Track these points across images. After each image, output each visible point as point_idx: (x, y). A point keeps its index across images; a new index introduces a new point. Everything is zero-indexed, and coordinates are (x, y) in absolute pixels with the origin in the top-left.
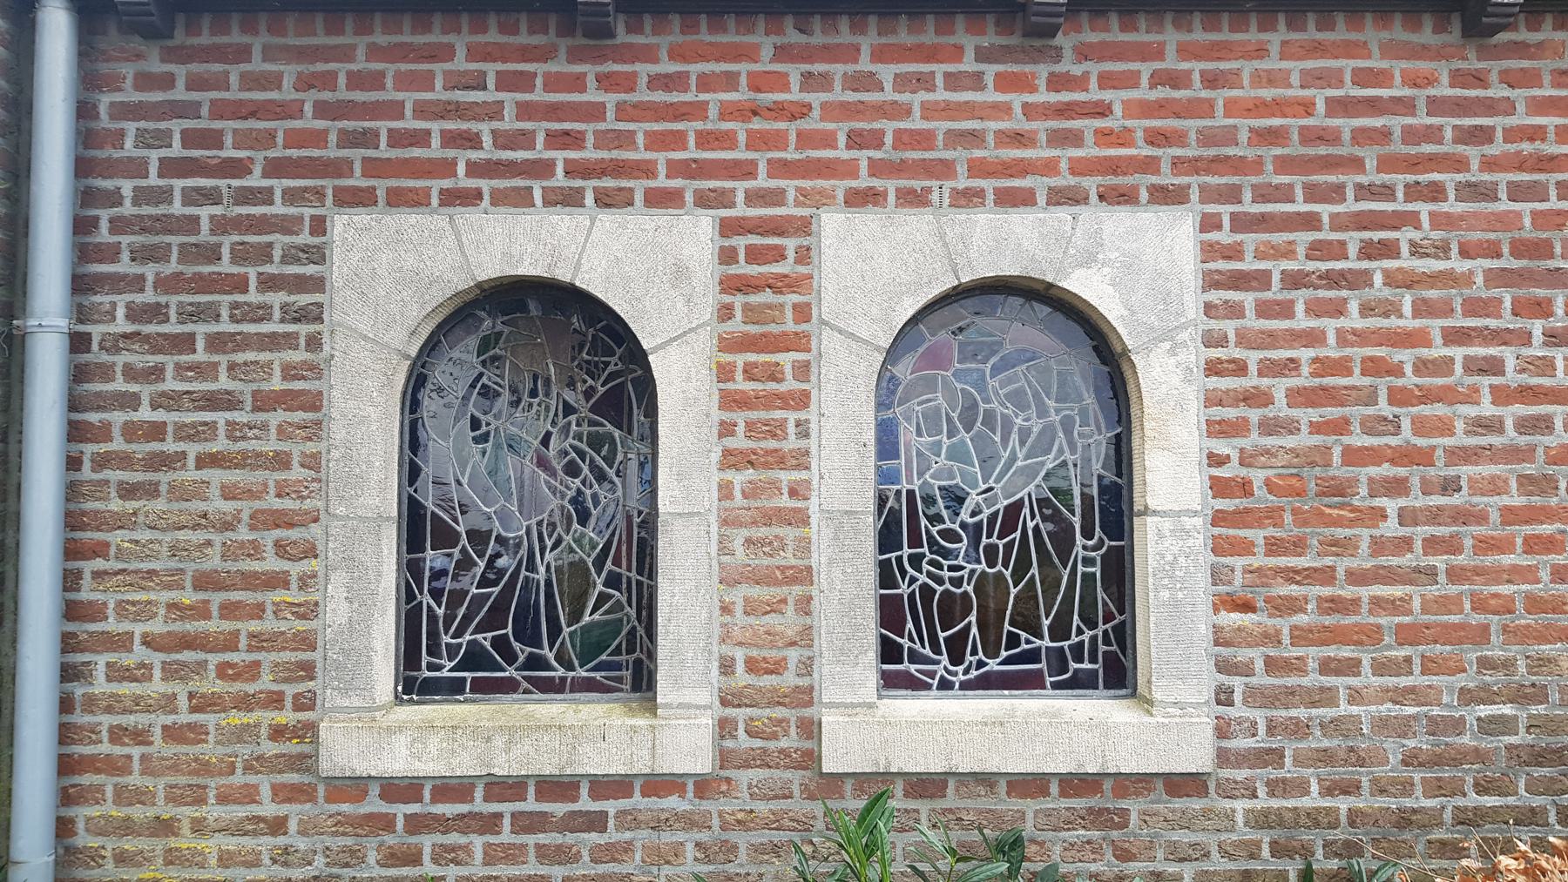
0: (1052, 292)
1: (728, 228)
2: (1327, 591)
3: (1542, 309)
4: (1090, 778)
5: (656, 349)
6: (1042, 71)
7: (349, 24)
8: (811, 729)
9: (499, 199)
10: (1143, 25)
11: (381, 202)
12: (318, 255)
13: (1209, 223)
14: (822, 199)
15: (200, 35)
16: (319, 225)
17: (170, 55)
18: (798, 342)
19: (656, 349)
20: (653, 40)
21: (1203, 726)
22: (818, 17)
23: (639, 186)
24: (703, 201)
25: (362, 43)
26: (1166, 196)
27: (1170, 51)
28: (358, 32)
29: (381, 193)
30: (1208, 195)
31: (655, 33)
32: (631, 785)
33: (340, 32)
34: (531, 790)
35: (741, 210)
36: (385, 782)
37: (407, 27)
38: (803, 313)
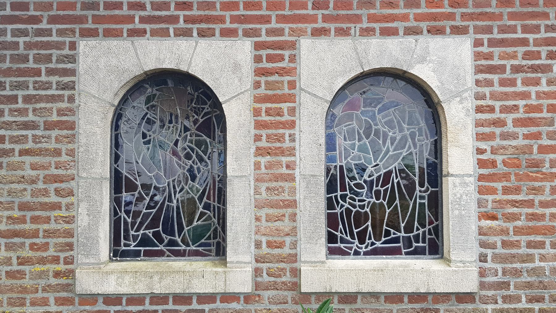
0: (406, 75)
1: (258, 46)
2: (530, 211)
5: (226, 102)
8: (296, 273)
9: (154, 33)
11: (101, 34)
12: (73, 59)
13: (478, 43)
14: (301, 33)
16: (73, 46)
18: (290, 98)
19: (226, 102)
24: (247, 34)
30: (478, 30)
34: (171, 300)
35: (264, 38)
36: (105, 296)
38: (292, 85)
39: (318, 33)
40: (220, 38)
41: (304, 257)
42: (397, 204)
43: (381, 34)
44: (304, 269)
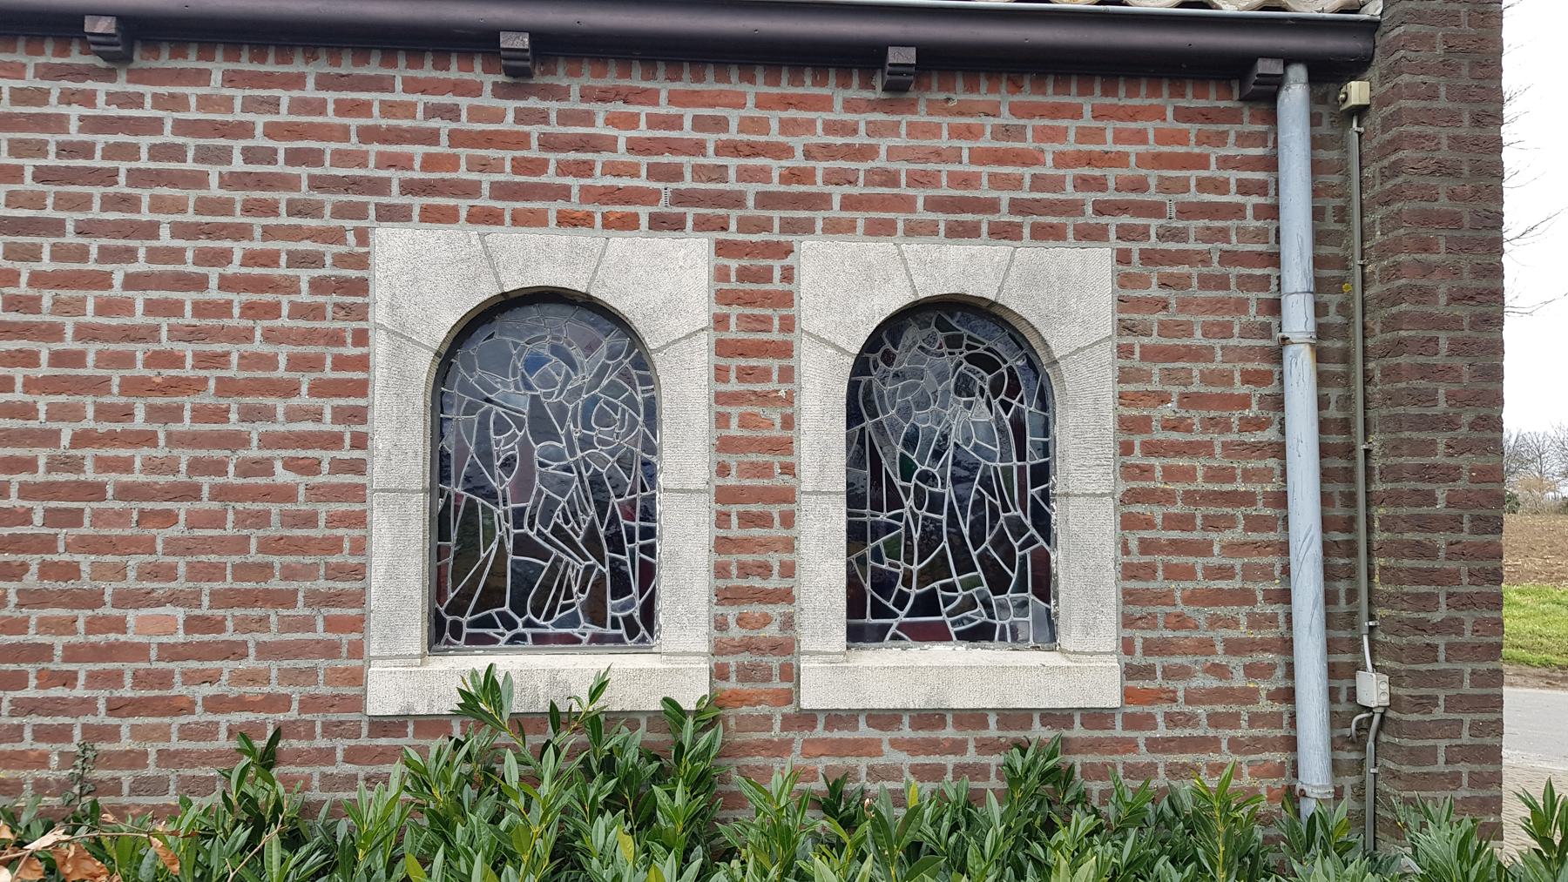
0: (993, 310)
1: (722, 249)
2: (334, 559)
3: (13, 304)
4: (844, 714)
5: (659, 350)
6: (905, 119)
7: (832, 80)
8: (790, 674)
9: (519, 220)
10: (1189, 92)
11: (900, 232)
12: (362, 262)
13: (1123, 258)
14: (806, 228)
15: (448, 70)
16: (363, 237)
17: (138, 77)
18: (785, 350)
19: (659, 350)
20: (1080, 100)
21: (1111, 668)
22: (246, 48)
23: (553, 208)
24: (702, 225)
25: (31, 62)
26: (1090, 235)
27: (217, 77)
28: (30, 53)
29: (860, 224)
30: (1125, 233)
31: (1080, 94)
32: (943, 718)
33: (824, 84)
34: (1077, 719)
35: (733, 235)
36: (915, 714)
37: (1189, 92)
38: (788, 325)
39: (833, 228)
40: (947, 240)
41: (806, 644)
42: (944, 547)
43: (1034, 236)
44: (806, 664)
